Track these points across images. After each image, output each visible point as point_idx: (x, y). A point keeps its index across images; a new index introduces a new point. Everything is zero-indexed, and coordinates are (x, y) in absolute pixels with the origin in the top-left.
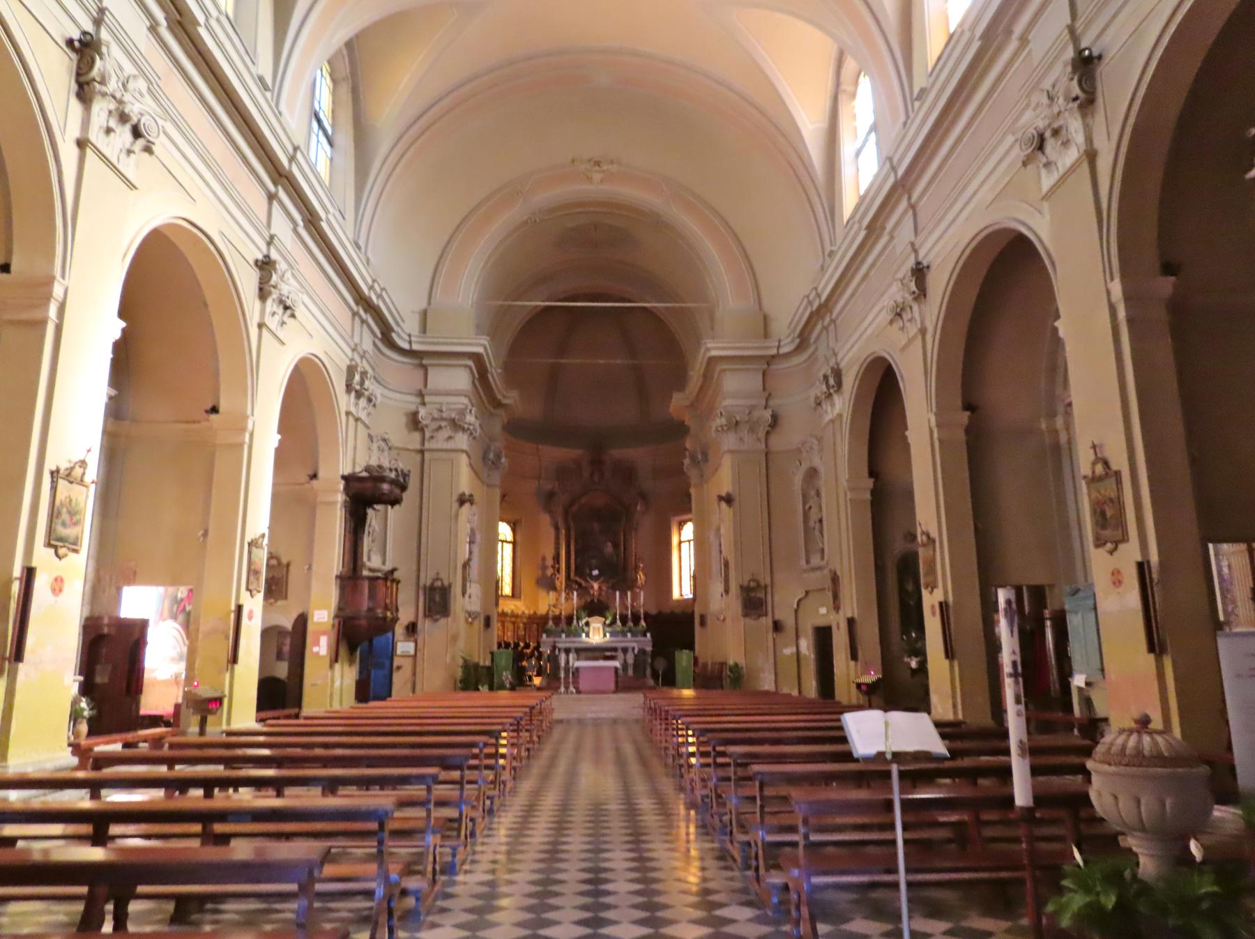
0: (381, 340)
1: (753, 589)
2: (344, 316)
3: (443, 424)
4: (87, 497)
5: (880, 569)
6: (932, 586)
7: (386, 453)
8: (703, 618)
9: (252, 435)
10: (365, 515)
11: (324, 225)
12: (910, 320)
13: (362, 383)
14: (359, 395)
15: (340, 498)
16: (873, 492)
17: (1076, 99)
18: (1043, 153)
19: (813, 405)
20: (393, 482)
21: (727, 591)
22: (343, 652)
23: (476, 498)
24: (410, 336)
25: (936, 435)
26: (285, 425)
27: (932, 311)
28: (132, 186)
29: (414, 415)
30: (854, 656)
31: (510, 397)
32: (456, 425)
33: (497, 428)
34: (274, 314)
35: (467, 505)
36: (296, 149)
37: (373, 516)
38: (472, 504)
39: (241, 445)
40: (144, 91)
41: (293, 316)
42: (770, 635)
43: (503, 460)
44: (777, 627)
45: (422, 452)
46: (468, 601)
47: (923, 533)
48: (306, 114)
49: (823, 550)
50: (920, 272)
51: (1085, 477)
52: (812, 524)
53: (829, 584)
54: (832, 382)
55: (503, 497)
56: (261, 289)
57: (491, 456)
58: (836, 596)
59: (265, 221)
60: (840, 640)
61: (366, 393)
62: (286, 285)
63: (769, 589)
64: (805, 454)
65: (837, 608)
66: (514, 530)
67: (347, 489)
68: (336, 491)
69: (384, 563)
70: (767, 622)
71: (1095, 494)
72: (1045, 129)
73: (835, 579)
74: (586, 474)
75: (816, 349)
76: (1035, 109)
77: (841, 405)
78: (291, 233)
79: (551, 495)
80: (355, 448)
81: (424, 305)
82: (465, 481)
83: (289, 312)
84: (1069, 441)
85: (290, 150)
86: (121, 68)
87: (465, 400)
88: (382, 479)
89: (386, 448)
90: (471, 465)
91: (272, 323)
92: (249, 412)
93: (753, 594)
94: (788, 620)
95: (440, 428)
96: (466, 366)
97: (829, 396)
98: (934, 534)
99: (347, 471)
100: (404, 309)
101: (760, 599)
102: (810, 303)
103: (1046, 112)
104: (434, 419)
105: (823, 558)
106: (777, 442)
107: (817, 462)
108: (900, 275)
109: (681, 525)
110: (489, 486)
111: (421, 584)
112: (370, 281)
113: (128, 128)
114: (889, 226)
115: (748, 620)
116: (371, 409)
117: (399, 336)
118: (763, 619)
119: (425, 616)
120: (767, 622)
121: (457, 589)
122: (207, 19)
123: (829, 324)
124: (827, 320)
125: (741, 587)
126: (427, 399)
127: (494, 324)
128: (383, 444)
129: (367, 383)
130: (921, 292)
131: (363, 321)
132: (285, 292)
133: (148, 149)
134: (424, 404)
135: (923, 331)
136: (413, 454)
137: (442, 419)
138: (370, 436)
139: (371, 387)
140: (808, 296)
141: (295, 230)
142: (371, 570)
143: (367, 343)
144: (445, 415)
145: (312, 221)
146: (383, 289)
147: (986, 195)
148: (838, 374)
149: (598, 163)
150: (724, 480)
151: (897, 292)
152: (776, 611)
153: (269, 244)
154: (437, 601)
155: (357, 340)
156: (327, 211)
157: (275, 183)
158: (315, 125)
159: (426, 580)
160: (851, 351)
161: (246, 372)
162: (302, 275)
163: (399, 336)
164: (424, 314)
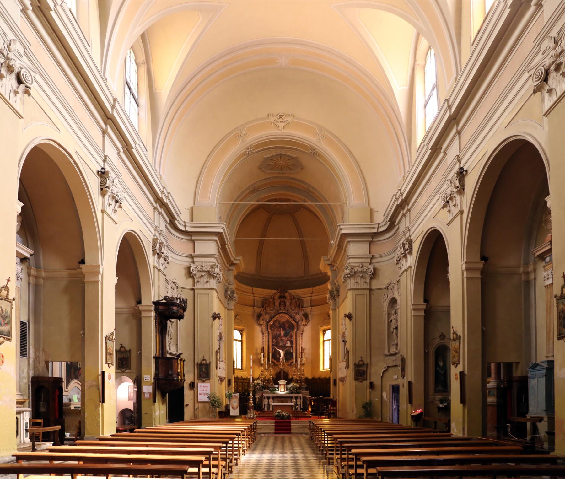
0: (169, 224)
1: (361, 366)
2: (149, 210)
3: (203, 274)
4: (12, 308)
5: (426, 354)
6: (457, 364)
7: (175, 290)
8: (335, 381)
9: (102, 276)
10: (167, 324)
11: (134, 151)
12: (455, 205)
13: (160, 250)
14: (159, 256)
15: (153, 314)
16: (426, 311)
17: (458, 187)
18: (547, 83)
19: (396, 261)
20: (178, 306)
21: (348, 367)
22: (158, 397)
23: (222, 316)
24: (184, 222)
25: (465, 275)
26: (120, 271)
27: (466, 202)
28: (21, 117)
29: (189, 268)
30: (410, 401)
31: (238, 260)
32: (211, 275)
33: (232, 279)
34: (110, 204)
35: (217, 319)
36: (115, 100)
37: (171, 325)
38: (219, 319)
39: (98, 282)
40: (22, 53)
41: (120, 207)
42: (368, 390)
43: (235, 295)
44: (372, 385)
45: (193, 289)
46: (219, 371)
47: (454, 333)
48: (122, 82)
49: (397, 344)
50: (462, 174)
51: (556, 296)
52: (392, 329)
53: (399, 363)
54: (407, 246)
55: (236, 316)
56: (102, 189)
57: (229, 293)
58: (403, 369)
59: (101, 148)
60: (404, 392)
61: (163, 255)
62: (116, 188)
63: (369, 367)
64: (390, 291)
65: (403, 376)
66: (242, 335)
67: (156, 310)
68: (151, 311)
69: (177, 351)
70: (367, 383)
71: (561, 306)
72: (550, 65)
73: (403, 360)
74: (277, 304)
75: (399, 228)
76: (543, 54)
77: (411, 261)
78: (116, 156)
79: (259, 316)
80: (159, 287)
81: (192, 205)
82: (217, 307)
83: (118, 204)
84: (535, 279)
85: (112, 101)
86: (5, 35)
87: (214, 260)
88: (173, 304)
89: (175, 288)
90: (218, 297)
91: (109, 210)
92: (100, 263)
93: (360, 368)
94: (377, 382)
95: (202, 276)
96: (214, 240)
97: (405, 256)
98: (460, 333)
99: (156, 299)
100: (181, 204)
101: (364, 371)
102: (397, 199)
103: (553, 53)
104: (198, 271)
105: (397, 349)
106: (376, 284)
107: (396, 296)
108: (449, 177)
109: (324, 332)
110: (228, 310)
111: (196, 363)
112: (162, 188)
113: (13, 76)
114: (444, 147)
115: (357, 382)
116: (166, 265)
117: (179, 222)
118: (365, 382)
119: (198, 379)
120: (367, 383)
121: (213, 365)
122: (55, 6)
123: (406, 212)
124: (406, 209)
125: (355, 364)
126: (195, 259)
127: (230, 214)
128: (174, 285)
129: (163, 249)
130: (461, 189)
131: (160, 213)
132: (115, 192)
133: (27, 92)
134: (193, 262)
135: (461, 212)
136: (189, 291)
137: (203, 271)
138: (166, 280)
139: (165, 252)
140: (396, 195)
141: (118, 154)
142: (170, 354)
143: (163, 226)
144: (204, 269)
145: (128, 148)
146: (169, 193)
147: (506, 119)
148: (410, 242)
149: (281, 116)
150: (347, 306)
151: (448, 188)
152: (372, 378)
153: (104, 161)
154: (204, 372)
155: (157, 224)
156: (135, 143)
157: (106, 124)
158: (127, 90)
159: (198, 360)
160: (417, 228)
161: (98, 240)
162: (123, 180)
163: (179, 222)
164: (192, 209)
